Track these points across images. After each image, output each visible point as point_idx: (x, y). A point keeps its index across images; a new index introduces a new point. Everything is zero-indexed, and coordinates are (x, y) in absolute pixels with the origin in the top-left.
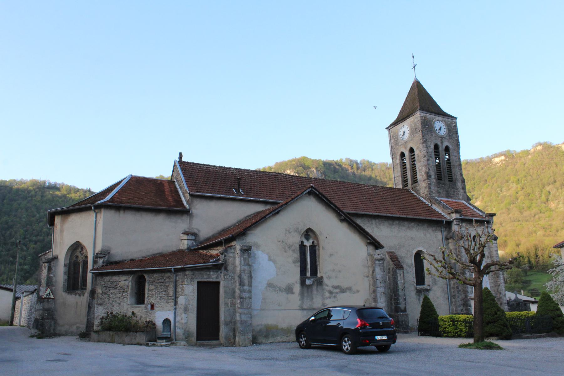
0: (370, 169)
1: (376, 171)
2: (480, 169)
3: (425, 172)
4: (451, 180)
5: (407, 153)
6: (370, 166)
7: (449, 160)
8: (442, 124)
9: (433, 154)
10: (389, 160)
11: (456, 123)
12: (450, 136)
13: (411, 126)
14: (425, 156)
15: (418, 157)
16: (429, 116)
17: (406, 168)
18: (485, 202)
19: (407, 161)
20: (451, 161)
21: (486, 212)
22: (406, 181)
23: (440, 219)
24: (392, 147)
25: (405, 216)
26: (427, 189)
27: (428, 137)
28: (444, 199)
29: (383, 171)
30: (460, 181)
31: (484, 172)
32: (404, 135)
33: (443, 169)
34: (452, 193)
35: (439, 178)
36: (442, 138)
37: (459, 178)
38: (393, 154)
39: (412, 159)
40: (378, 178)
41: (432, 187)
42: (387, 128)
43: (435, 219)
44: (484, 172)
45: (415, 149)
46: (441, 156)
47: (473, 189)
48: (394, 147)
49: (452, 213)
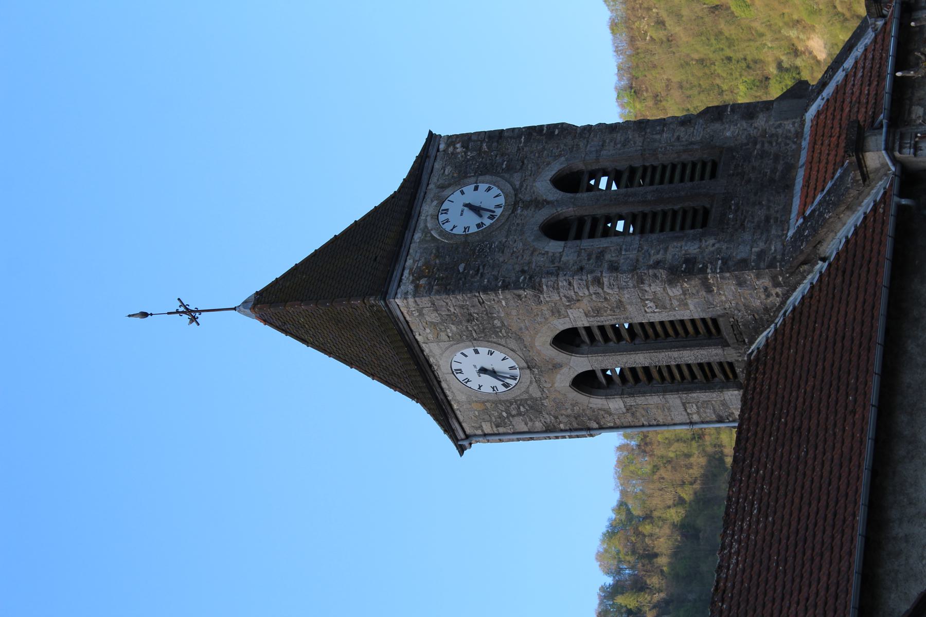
0: (647, 529)
1: (656, 502)
2: (661, 35)
3: (671, 282)
4: (708, 168)
5: (580, 363)
6: (628, 527)
7: (616, 176)
8: (456, 201)
9: (586, 243)
10: (610, 442)
11: (452, 140)
12: (509, 169)
13: (458, 340)
14: (598, 282)
15: (598, 312)
16: (414, 259)
17: (646, 369)
18: (813, 12)
19: (614, 363)
20: (623, 165)
21: (862, 11)
22: (706, 369)
23: (891, 221)
24: (551, 430)
25: (874, 384)
26: (750, 276)
28: (796, 202)
29: (656, 468)
30: (717, 126)
31: (679, 16)
32: (493, 373)
34: (556, 152)
35: (698, 220)
36: (516, 203)
37: (699, 133)
38: (583, 427)
39: (606, 339)
40: (687, 494)
41: (742, 252)
42: (461, 450)
43: (889, 243)
44: (679, 16)
45: (561, 325)
46: (600, 212)
47: (750, 65)
48: (549, 419)
49: (860, 165)
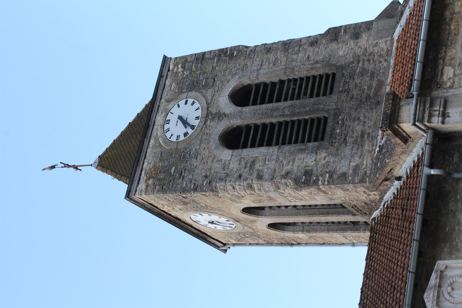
14: (251, 187)
22: (354, 223)
27: (199, 169)
30: (334, 46)
33: (293, 114)
36: (210, 115)
37: (320, 53)
41: (344, 166)
